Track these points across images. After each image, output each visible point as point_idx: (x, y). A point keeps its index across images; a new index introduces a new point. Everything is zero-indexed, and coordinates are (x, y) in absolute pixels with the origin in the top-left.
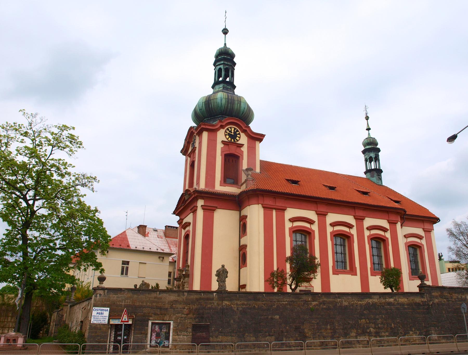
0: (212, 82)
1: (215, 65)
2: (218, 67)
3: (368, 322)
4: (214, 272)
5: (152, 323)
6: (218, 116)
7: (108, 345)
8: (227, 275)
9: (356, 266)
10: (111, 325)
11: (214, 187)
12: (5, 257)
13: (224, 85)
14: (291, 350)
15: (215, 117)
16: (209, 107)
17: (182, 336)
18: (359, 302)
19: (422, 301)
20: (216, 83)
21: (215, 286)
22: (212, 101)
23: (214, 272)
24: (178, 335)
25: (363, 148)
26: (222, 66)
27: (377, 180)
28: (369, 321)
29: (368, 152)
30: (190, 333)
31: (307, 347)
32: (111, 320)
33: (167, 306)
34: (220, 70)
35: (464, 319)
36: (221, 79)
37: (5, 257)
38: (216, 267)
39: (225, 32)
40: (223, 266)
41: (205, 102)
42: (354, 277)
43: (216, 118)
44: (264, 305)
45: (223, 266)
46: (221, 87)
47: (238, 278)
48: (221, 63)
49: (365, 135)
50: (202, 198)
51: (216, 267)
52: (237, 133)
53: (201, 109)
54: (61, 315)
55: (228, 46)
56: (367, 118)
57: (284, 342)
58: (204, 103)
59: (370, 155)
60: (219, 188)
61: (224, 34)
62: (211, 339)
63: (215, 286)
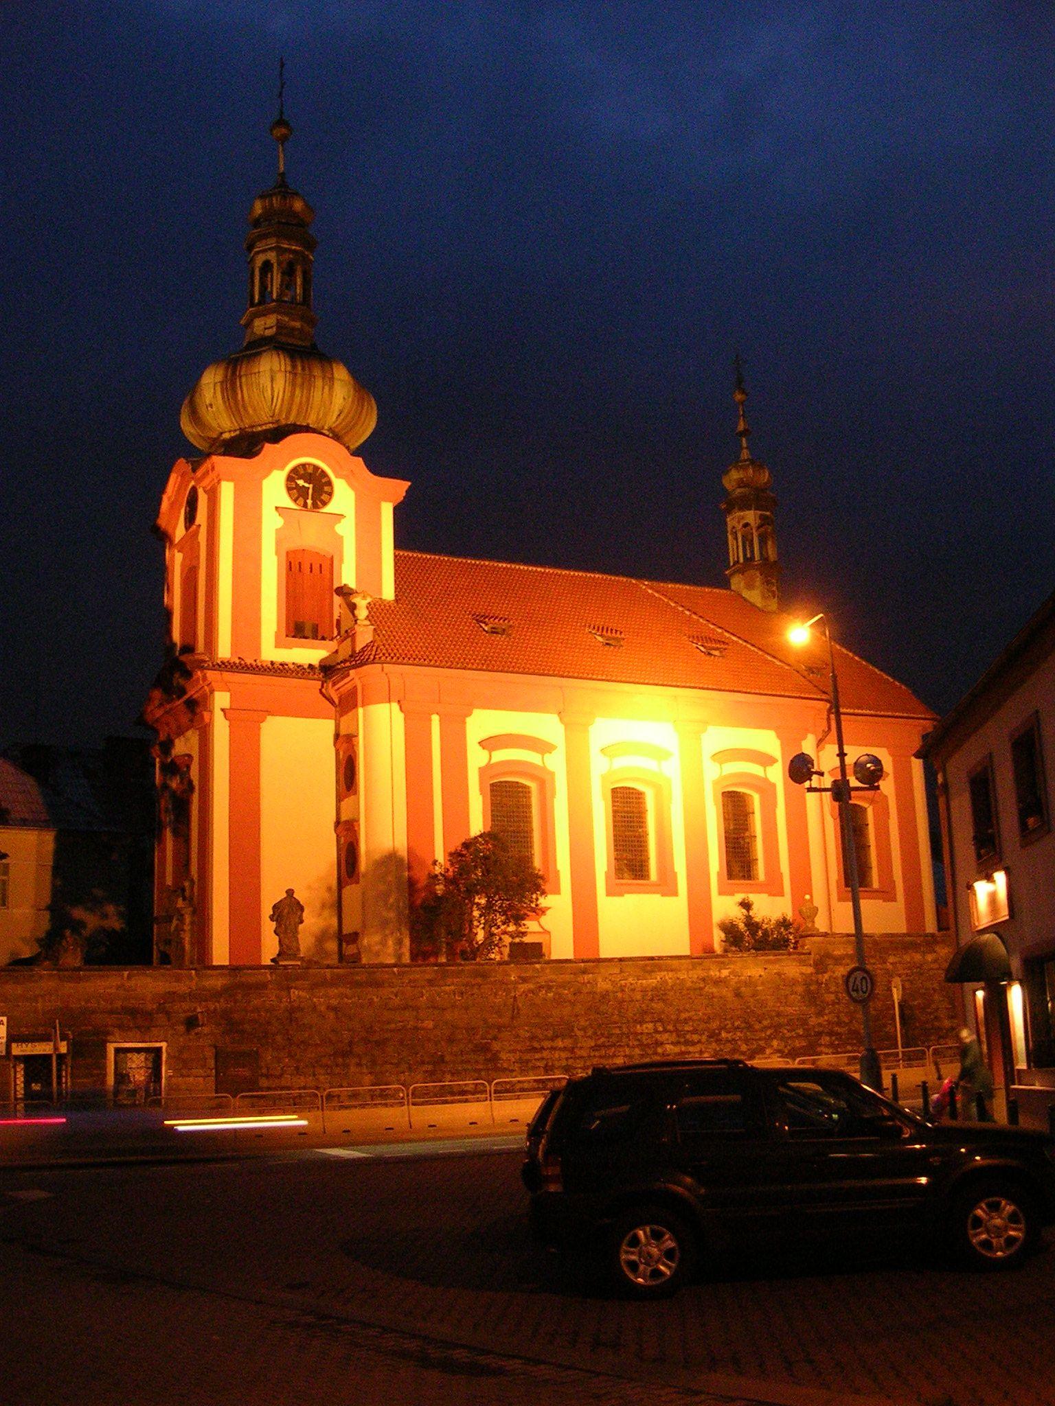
3: (661, 1029)
4: (267, 910)
5: (117, 1050)
7: (12, 1106)
8: (301, 916)
9: (676, 869)
10: (17, 1058)
11: (257, 649)
12: (629, 1106)
13: (280, 317)
14: (466, 1101)
16: (234, 373)
17: (191, 1079)
18: (638, 980)
19: (802, 974)
21: (270, 946)
23: (267, 910)
24: (182, 1076)
26: (272, 256)
27: (764, 597)
28: (664, 1028)
30: (211, 1070)
31: (495, 1093)
32: (14, 1045)
33: (150, 1006)
37: (629, 1106)
38: (270, 896)
40: (290, 892)
42: (668, 900)
44: (396, 996)
45: (290, 892)
46: (272, 327)
51: (270, 896)
52: (323, 481)
54: (467, 1030)
57: (447, 1083)
60: (270, 652)
62: (264, 1082)
63: (270, 946)
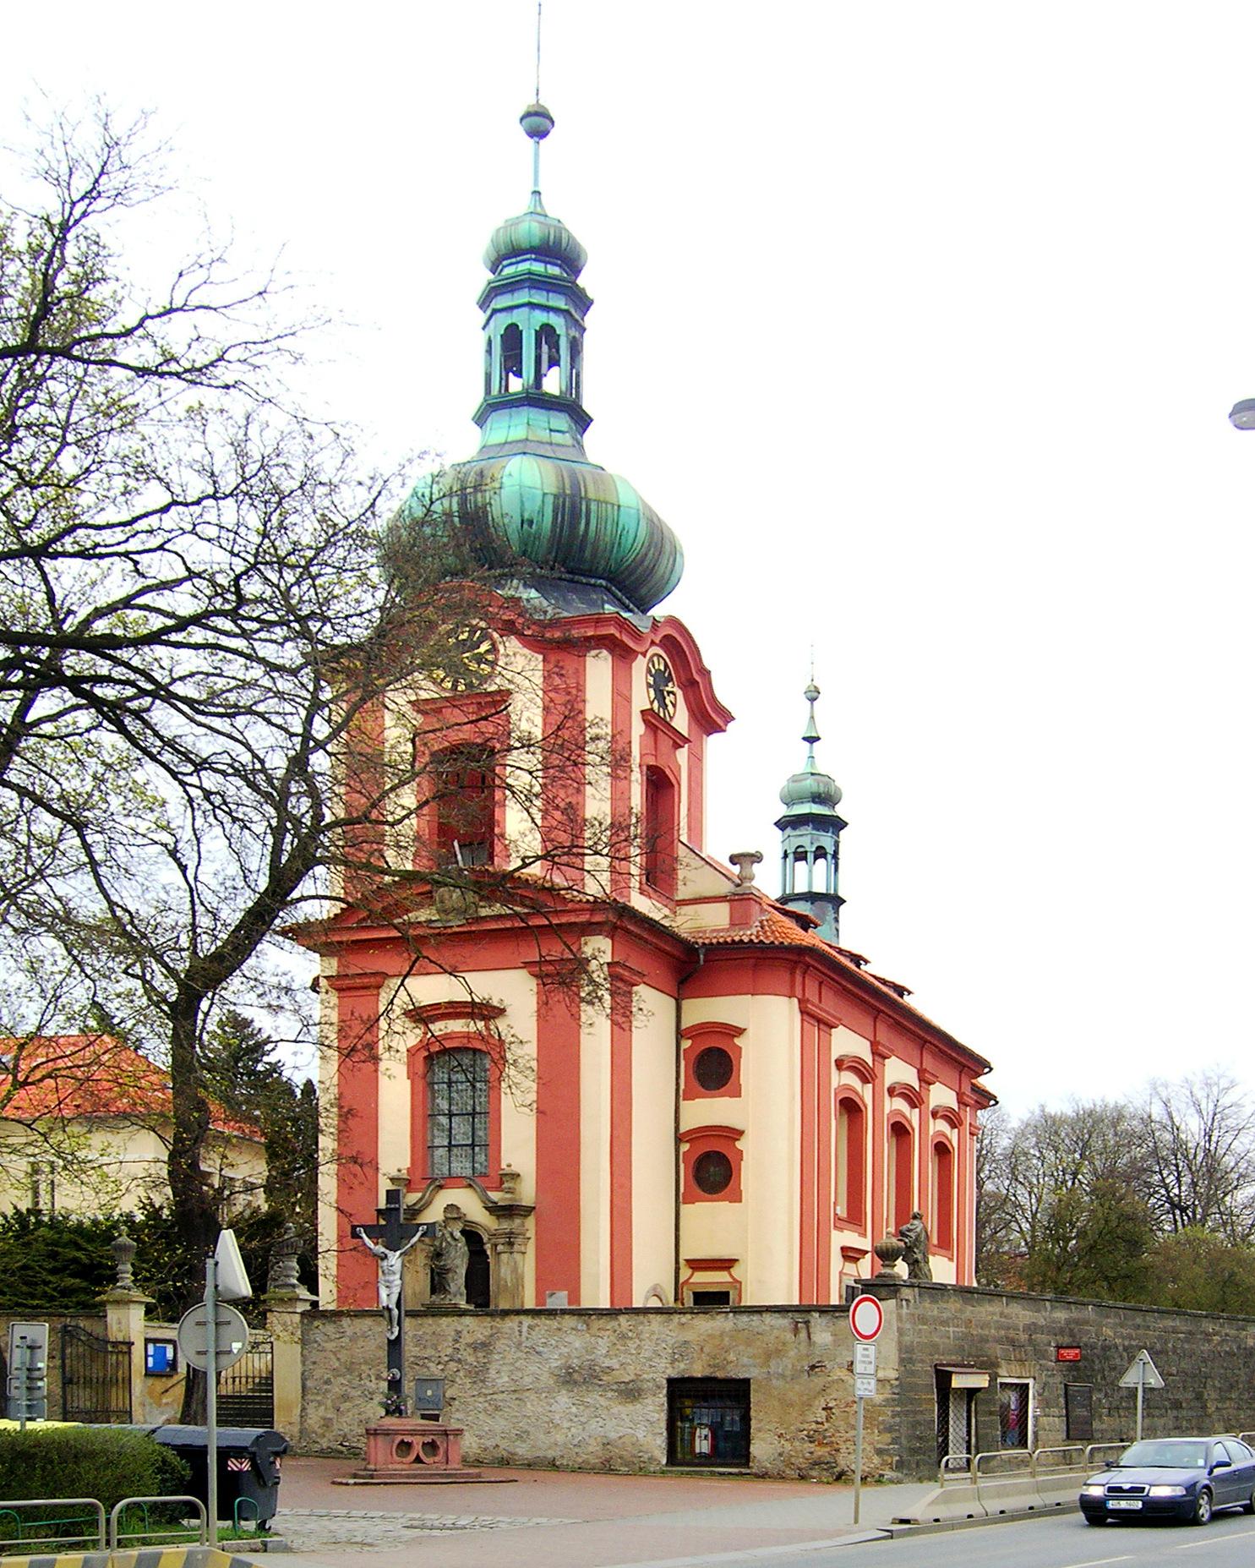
0: (476, 398)
1: (484, 303)
2: (503, 321)
6: (593, 581)
15: (576, 578)
16: (574, 525)
20: (495, 405)
22: (593, 507)
25: (782, 811)
29: (814, 829)
34: (512, 337)
35: (46, 1506)
36: (516, 385)
39: (538, 124)
41: (556, 497)
43: (594, 585)
47: (681, 1242)
48: (551, 303)
49: (793, 761)
50: (612, 931)
53: (531, 523)
55: (555, 209)
56: (813, 695)
58: (550, 500)
59: (818, 840)
61: (532, 137)
